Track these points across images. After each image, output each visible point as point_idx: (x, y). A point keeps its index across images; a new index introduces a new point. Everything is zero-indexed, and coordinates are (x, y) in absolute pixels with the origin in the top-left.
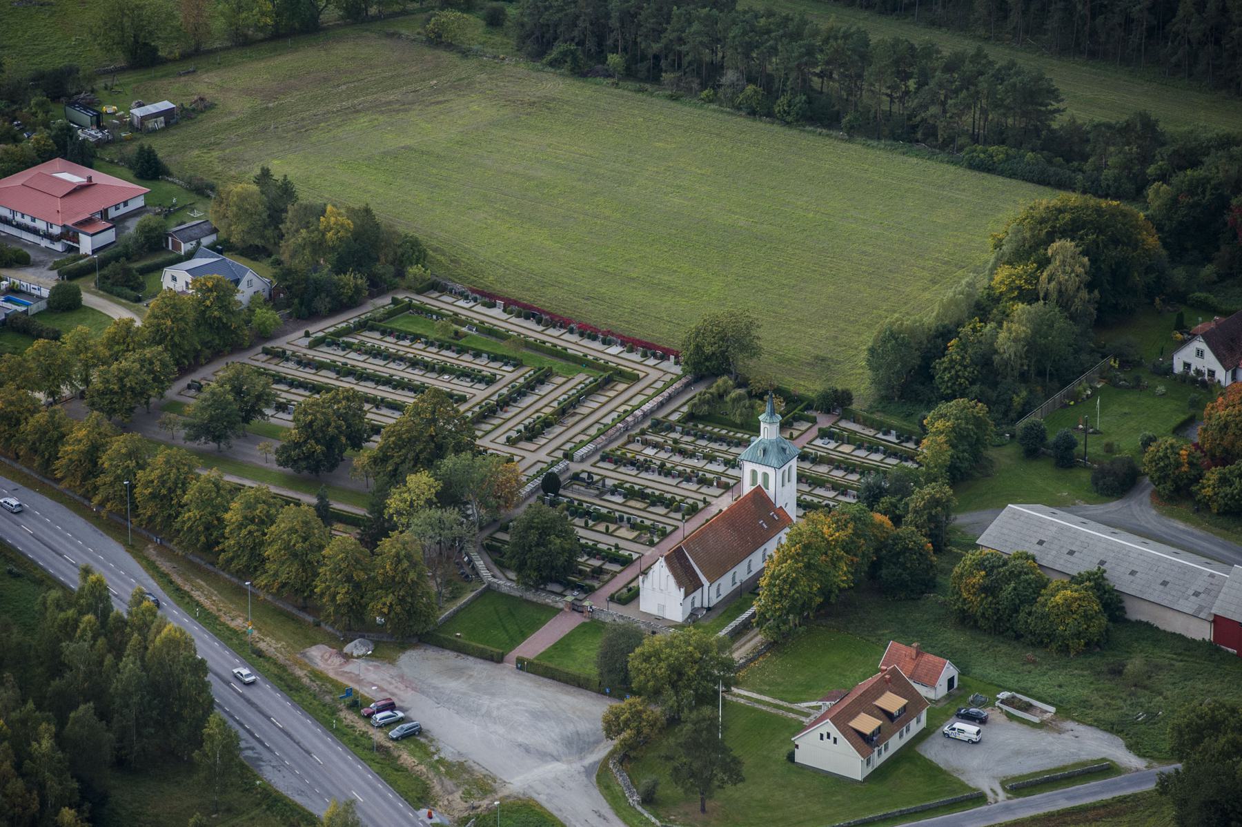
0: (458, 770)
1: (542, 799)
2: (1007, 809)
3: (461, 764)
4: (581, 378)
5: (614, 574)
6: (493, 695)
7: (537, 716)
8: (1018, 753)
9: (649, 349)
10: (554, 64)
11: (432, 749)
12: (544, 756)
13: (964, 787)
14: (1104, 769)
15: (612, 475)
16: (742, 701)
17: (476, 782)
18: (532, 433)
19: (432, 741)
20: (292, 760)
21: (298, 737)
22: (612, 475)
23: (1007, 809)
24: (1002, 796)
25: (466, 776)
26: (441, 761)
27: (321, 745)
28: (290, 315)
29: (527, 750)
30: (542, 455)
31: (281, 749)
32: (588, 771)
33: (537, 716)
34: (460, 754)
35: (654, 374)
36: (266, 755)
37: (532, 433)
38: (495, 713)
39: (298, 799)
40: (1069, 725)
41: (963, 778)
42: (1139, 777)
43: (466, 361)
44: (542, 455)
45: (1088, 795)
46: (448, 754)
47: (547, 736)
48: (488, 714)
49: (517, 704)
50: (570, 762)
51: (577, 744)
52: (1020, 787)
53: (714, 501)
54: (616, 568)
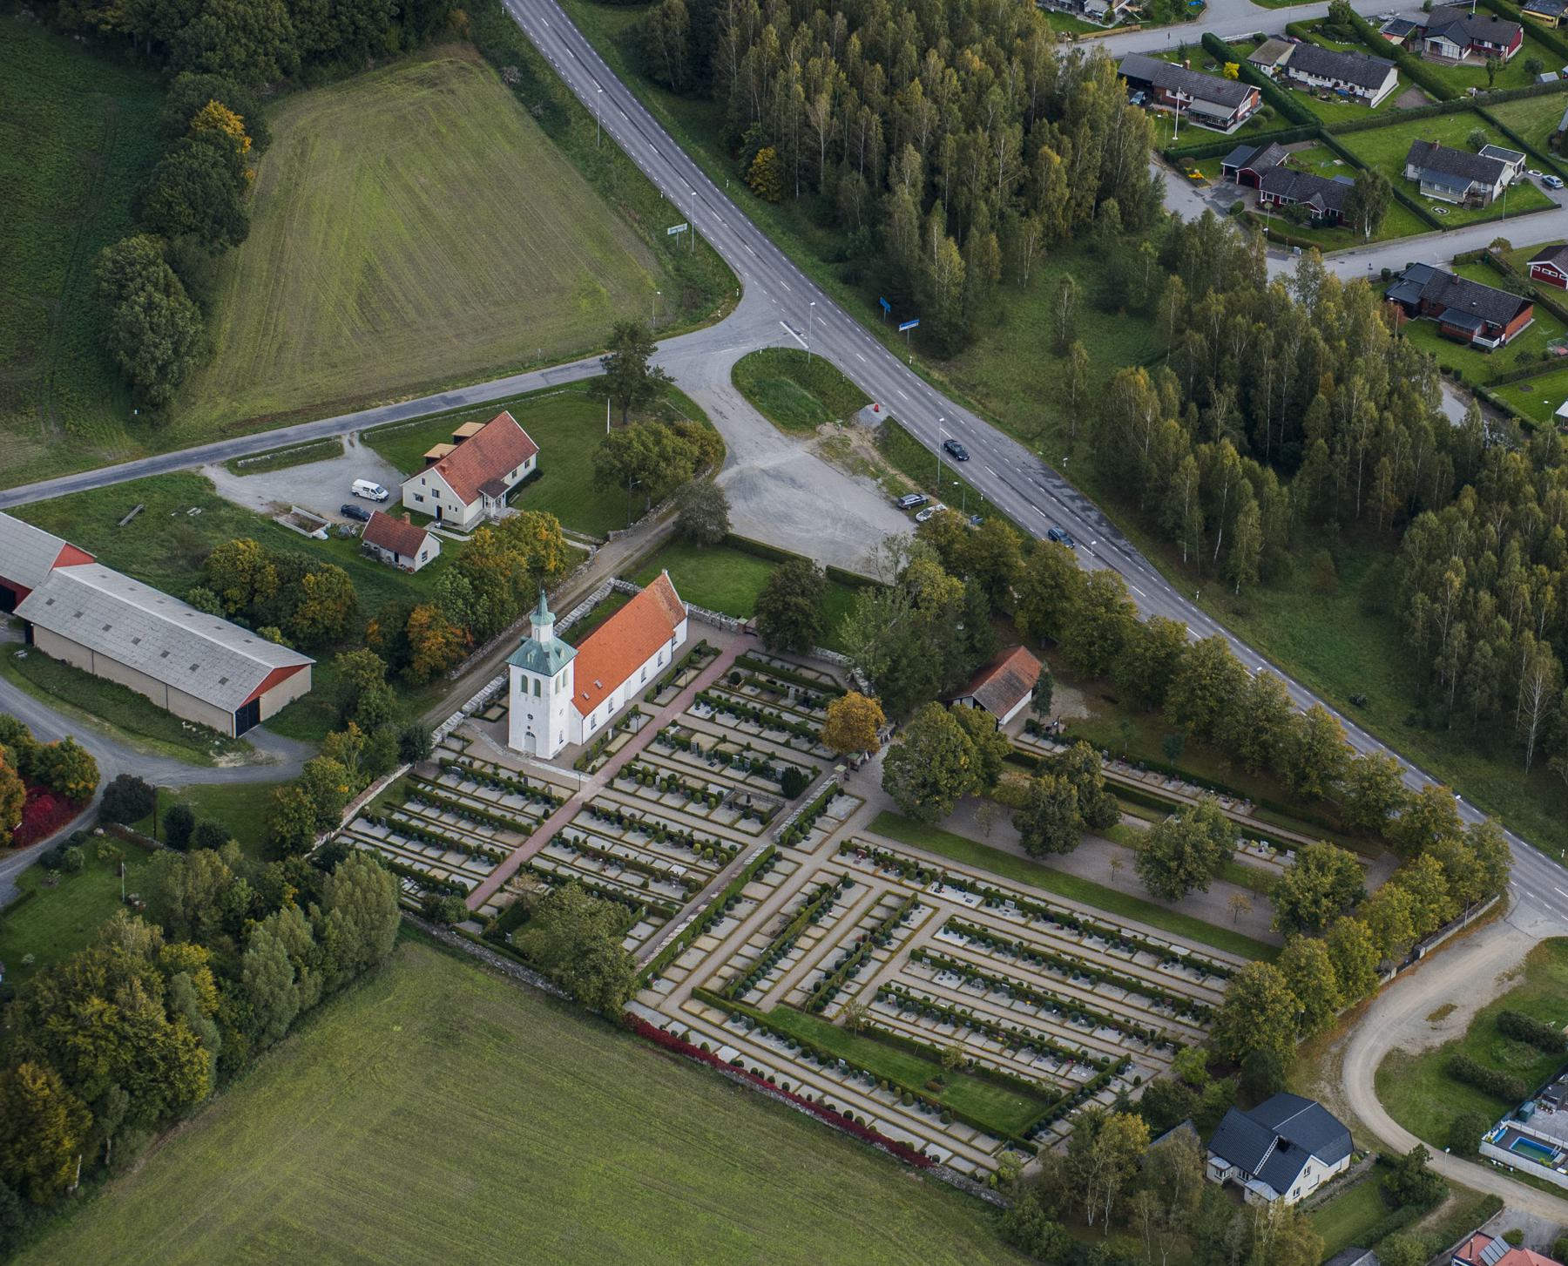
0: (857, 467)
1: (775, 433)
2: (343, 427)
3: (855, 473)
4: (764, 998)
5: (715, 686)
6: (833, 542)
7: (785, 518)
8: (321, 482)
9: (676, 1047)
10: (100, 1169)
11: (884, 489)
12: (777, 475)
13: (378, 451)
14: (238, 468)
15: (717, 825)
16: (582, 536)
17: (839, 455)
18: (821, 901)
19: (887, 498)
20: (1015, 473)
21: (1016, 496)
22: (717, 825)
23: (343, 427)
24: (345, 441)
25: (849, 461)
26: (875, 477)
27: (991, 484)
28: (1172, 672)
29: (793, 481)
30: (809, 864)
31: (1027, 483)
32: (734, 460)
33: (785, 518)
34: (858, 483)
35: (671, 1006)
36: (1042, 480)
37: (821, 901)
38: (828, 522)
39: (1001, 435)
40: (262, 510)
41: (378, 457)
42: (209, 457)
43: (924, 1031)
44: (809, 864)
45: (262, 440)
46: (870, 484)
47: (776, 496)
48: (835, 520)
49: (808, 531)
50: (752, 468)
51: (748, 486)
52: (328, 450)
53: (601, 790)
54: (714, 694)
